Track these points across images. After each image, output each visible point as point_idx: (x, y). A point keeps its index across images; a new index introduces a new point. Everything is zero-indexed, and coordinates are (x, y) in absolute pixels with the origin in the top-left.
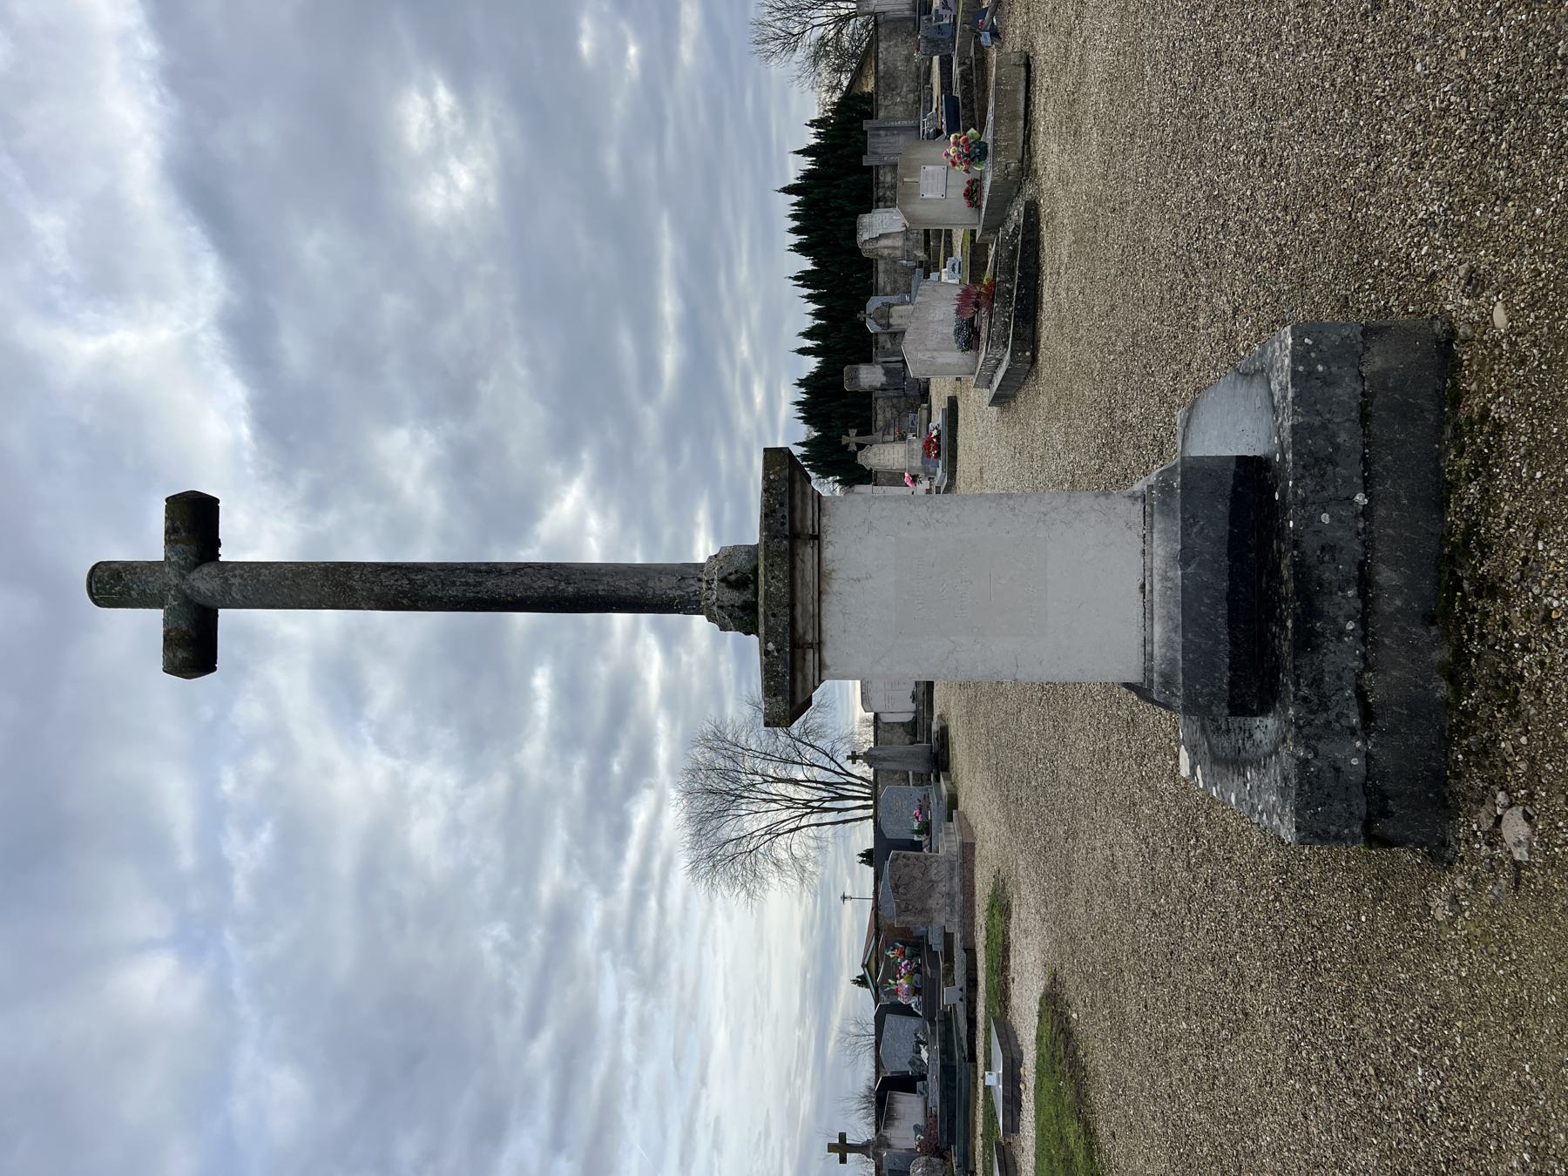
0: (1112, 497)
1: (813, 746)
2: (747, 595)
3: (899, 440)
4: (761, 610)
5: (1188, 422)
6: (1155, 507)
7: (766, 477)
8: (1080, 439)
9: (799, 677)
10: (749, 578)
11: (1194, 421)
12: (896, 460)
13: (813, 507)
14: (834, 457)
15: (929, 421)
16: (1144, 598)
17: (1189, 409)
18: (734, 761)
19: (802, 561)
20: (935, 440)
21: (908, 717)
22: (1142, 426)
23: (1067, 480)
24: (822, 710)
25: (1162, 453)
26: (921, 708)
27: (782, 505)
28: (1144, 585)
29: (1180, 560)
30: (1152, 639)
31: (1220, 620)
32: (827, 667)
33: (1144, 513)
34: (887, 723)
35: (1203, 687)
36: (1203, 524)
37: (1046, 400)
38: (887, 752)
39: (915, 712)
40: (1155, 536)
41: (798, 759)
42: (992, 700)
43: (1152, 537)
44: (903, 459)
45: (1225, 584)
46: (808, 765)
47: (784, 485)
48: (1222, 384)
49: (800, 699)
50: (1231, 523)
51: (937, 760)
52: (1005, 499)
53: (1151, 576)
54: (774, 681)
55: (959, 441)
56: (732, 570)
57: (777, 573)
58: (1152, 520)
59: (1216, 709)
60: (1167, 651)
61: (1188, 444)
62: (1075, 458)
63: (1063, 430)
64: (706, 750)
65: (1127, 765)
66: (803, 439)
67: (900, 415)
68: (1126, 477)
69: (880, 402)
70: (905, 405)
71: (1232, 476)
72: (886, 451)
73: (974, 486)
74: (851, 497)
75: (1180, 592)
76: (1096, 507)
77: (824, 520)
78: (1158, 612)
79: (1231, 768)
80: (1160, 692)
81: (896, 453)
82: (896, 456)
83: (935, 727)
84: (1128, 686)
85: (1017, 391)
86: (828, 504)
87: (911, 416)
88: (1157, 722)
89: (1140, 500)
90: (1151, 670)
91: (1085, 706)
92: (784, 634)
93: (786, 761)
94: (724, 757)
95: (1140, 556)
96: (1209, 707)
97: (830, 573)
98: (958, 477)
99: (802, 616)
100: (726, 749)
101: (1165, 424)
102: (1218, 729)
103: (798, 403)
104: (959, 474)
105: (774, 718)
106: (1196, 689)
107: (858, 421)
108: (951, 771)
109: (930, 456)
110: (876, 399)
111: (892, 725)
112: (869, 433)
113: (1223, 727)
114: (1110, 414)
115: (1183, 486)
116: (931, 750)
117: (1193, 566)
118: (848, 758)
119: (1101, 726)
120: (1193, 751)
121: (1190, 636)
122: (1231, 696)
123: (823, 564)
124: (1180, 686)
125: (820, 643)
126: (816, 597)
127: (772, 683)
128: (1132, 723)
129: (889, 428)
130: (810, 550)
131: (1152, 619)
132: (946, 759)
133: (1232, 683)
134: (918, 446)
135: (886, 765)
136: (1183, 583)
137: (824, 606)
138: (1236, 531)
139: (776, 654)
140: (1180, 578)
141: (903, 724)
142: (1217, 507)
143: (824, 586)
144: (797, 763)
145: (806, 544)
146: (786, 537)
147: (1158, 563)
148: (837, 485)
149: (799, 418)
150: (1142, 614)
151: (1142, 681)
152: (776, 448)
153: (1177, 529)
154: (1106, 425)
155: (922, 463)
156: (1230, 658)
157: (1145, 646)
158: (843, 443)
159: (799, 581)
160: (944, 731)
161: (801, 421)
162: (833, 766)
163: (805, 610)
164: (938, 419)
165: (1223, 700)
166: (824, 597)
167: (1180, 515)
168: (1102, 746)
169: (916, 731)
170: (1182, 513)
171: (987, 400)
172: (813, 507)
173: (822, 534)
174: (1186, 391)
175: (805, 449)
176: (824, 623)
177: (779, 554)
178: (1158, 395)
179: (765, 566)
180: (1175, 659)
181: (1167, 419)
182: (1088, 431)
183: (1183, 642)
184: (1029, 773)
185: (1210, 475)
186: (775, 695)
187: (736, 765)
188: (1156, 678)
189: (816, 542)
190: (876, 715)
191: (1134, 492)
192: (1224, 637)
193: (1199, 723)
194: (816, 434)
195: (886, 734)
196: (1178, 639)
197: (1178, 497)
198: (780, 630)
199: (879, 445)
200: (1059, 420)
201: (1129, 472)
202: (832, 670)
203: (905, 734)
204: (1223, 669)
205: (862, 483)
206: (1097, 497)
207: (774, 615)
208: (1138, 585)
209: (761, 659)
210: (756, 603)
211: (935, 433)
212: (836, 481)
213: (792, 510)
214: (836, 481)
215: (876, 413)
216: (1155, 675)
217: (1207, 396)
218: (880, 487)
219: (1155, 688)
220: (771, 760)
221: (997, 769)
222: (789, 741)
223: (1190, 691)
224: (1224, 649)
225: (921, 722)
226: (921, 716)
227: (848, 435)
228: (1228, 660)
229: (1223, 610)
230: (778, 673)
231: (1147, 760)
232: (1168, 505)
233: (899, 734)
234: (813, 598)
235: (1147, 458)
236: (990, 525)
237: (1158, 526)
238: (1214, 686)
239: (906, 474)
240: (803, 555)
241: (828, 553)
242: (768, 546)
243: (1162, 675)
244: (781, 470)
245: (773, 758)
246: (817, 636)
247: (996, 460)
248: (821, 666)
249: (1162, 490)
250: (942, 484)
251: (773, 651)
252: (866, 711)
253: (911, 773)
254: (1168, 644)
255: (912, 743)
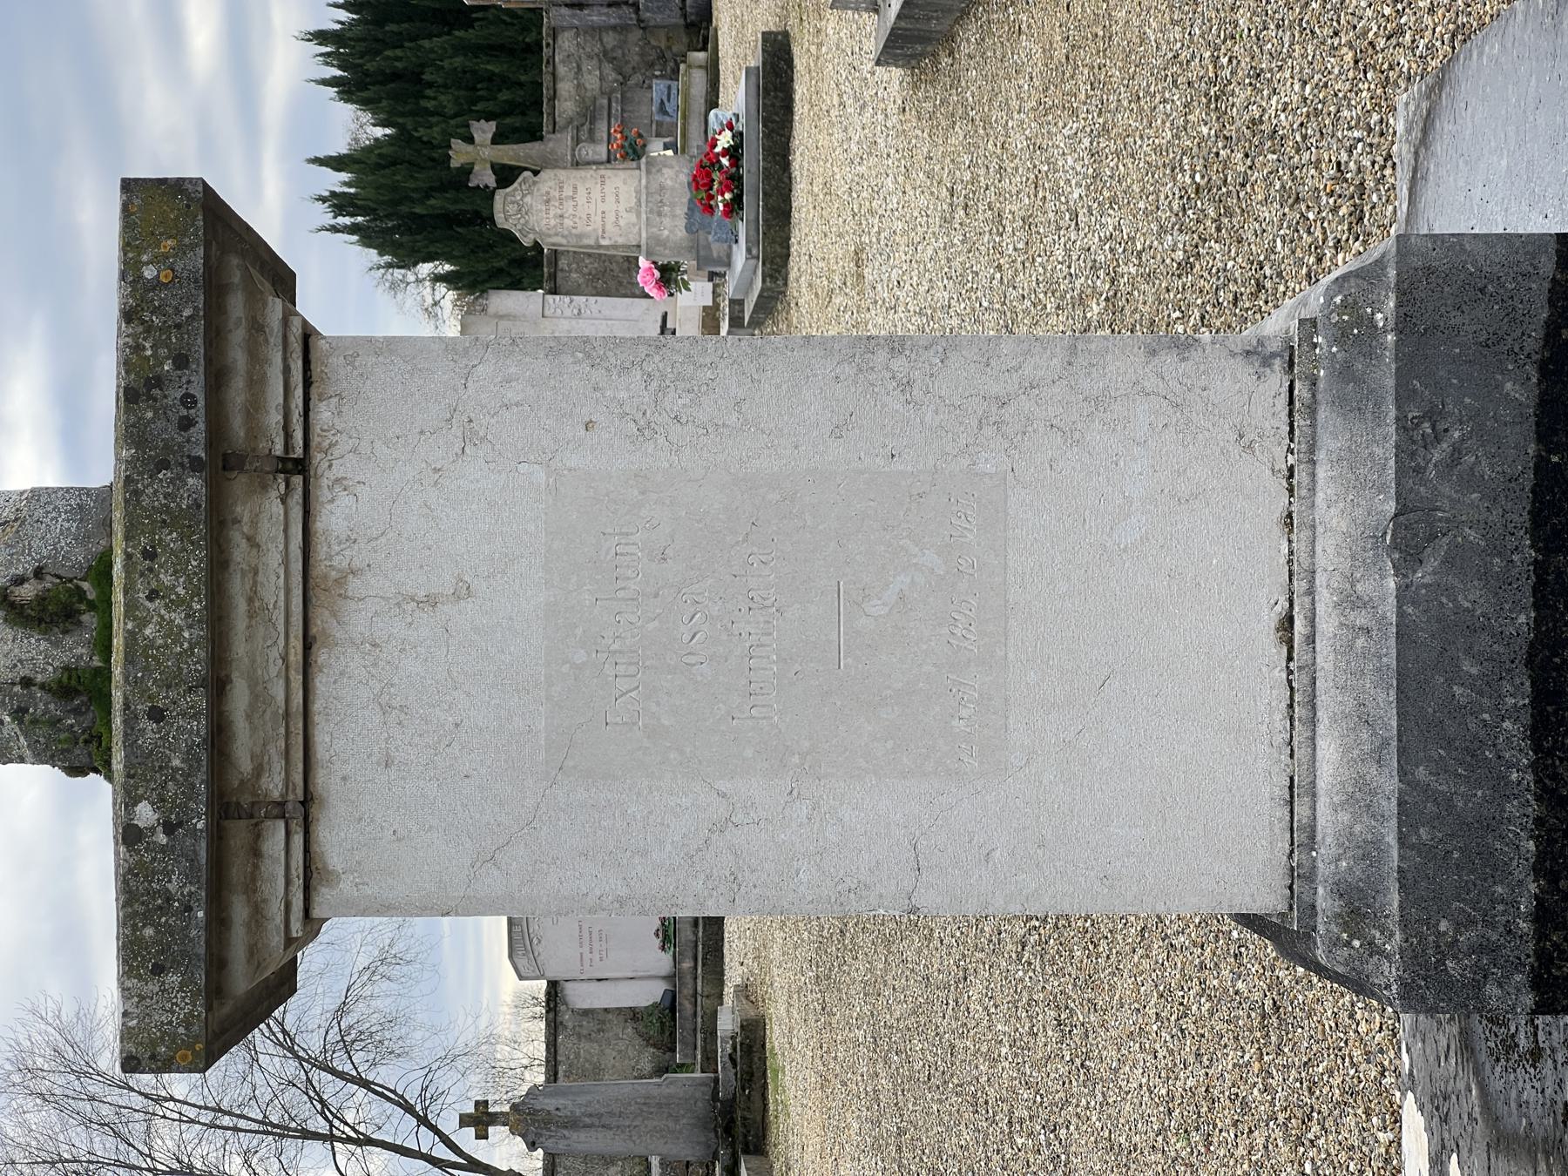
0: (1196, 355)
1: (365, 1084)
2: (75, 649)
3: (624, 157)
4: (117, 696)
5: (1426, 127)
6: (1321, 385)
7: (130, 271)
8: (1132, 171)
9: (239, 911)
10: (80, 593)
11: (1444, 126)
12: (611, 218)
13: (287, 370)
14: (432, 202)
15: (712, 103)
16: (1290, 659)
17: (1431, 89)
18: (117, 1134)
19: (252, 541)
20: (725, 161)
21: (648, 994)
22: (1304, 137)
23: (1096, 293)
24: (395, 972)
25: (1361, 219)
26: (687, 965)
27: (181, 362)
28: (1290, 619)
29: (1395, 546)
30: (1313, 783)
31: (1507, 724)
32: (330, 878)
33: (1291, 402)
34: (586, 1013)
35: (1458, 926)
36: (1462, 440)
37: (1037, 49)
38: (582, 1100)
39: (670, 978)
40: (1321, 473)
41: (320, 1125)
42: (888, 943)
43: (1313, 475)
44: (633, 218)
45: (1522, 619)
46: (349, 1140)
47: (189, 299)
48: (1520, 17)
49: (241, 981)
50: (1544, 435)
51: (733, 1120)
52: (882, 356)
53: (1311, 592)
54: (156, 926)
55: (796, 165)
56: (25, 566)
57: (166, 579)
58: (1313, 426)
59: (1497, 991)
60: (1356, 819)
61: (1428, 194)
62: (1118, 227)
63: (1086, 142)
64: (30, 1103)
65: (1260, 1141)
66: (340, 147)
67: (626, 82)
68: (1260, 287)
69: (566, 42)
70: (642, 55)
71: (1545, 296)
72: (581, 191)
73: (837, 300)
74: (485, 330)
75: (1393, 642)
76: (1151, 383)
77: (323, 414)
78: (1329, 702)
79: (1542, 1166)
80: (1335, 943)
81: (611, 199)
82: (610, 205)
83: (727, 1023)
84: (1249, 921)
85: (956, 21)
86: (336, 361)
87: (659, 86)
88: (1344, 1015)
89: (1277, 362)
90: (1310, 877)
91: (1145, 964)
92: (187, 776)
93: (282, 1132)
94: (87, 1122)
95: (1277, 532)
96: (1478, 986)
97: (341, 582)
98: (793, 275)
99: (249, 717)
100: (92, 1099)
101: (1370, 130)
102: (1510, 1045)
103: (321, 37)
104: (797, 264)
105: (153, 1044)
106: (1439, 934)
107: (504, 96)
108: (773, 1153)
109: (710, 209)
110: (554, 33)
111: (598, 1018)
112: (533, 134)
113: (1523, 1042)
114: (1217, 100)
115: (1404, 322)
116: (715, 1092)
117: (1432, 563)
118: (465, 1121)
119: (1188, 1024)
120: (1438, 1110)
121: (1421, 773)
122: (1541, 954)
123: (320, 551)
124: (1393, 924)
125: (308, 800)
126: (296, 656)
127: (149, 932)
128: (1275, 1015)
129: (593, 121)
130: (277, 508)
131: (1313, 722)
132: (759, 1118)
133: (1542, 915)
134: (675, 174)
135: (584, 1141)
136: (1401, 614)
137: (321, 684)
138: (1555, 459)
139: (162, 839)
140: (1392, 600)
141: (633, 1015)
142: (1499, 386)
143: (321, 619)
144: (316, 1136)
145: (265, 488)
146: (196, 465)
147: (1330, 555)
148: (441, 288)
149: (325, 82)
150: (1284, 705)
151: (1282, 907)
152: (162, 181)
153: (1386, 451)
154: (1205, 130)
155: (688, 228)
156: (1536, 838)
157: (1291, 803)
158: (454, 164)
159: (241, 606)
160: (753, 1037)
161: (332, 91)
162: (427, 1141)
163: (259, 696)
164: (736, 97)
165: (1518, 966)
166: (321, 656)
167: (1392, 413)
168: (1190, 1083)
169: (673, 1034)
170: (1398, 408)
171: (873, 46)
172: (287, 370)
173: (317, 457)
174: (1428, 33)
175: (345, 176)
176: (321, 738)
177: (172, 519)
178: (1350, 45)
179: (129, 556)
180: (1377, 843)
181: (1376, 117)
182: (1158, 150)
183: (1400, 791)
184: (989, 1159)
185: (1482, 290)
186: (158, 970)
187: (123, 1147)
188: (1325, 901)
189: (297, 480)
190: (554, 990)
191: (1261, 342)
192: (1520, 776)
193: (1455, 1029)
194: (379, 132)
195: (585, 1045)
196: (1389, 784)
197: (1389, 356)
198: (176, 762)
199: (562, 174)
200: (1074, 113)
201: (1268, 272)
202: (346, 886)
203: (638, 1041)
204: (1519, 874)
205: (516, 285)
206: (1153, 353)
207: (156, 715)
208: (1271, 618)
209: (117, 853)
210: (104, 674)
211: (725, 140)
212: (437, 278)
213: (217, 378)
214: (437, 278)
215: (554, 74)
216: (1320, 890)
217: (1480, 54)
218: (567, 299)
219: (1321, 928)
220: (236, 1129)
221: (899, 1149)
222: (291, 1067)
223: (1422, 938)
224: (1521, 810)
225: (688, 1006)
226: (688, 991)
227: (470, 140)
228: (1531, 845)
229: (1517, 694)
230: (169, 898)
231: (1316, 1129)
232: (1358, 381)
233: (622, 1046)
234: (285, 659)
235: (1318, 233)
236: (837, 432)
237: (1329, 444)
238: (1493, 926)
239: (643, 262)
240: (254, 523)
241: (334, 517)
242: (136, 493)
243: (1342, 890)
244: (181, 250)
245: (242, 1124)
246: (298, 778)
247: (899, 226)
248: (312, 874)
249: (1341, 335)
250: (747, 293)
251: (153, 829)
252: (521, 978)
253: (655, 1161)
254: (1359, 797)
255: (661, 1070)
